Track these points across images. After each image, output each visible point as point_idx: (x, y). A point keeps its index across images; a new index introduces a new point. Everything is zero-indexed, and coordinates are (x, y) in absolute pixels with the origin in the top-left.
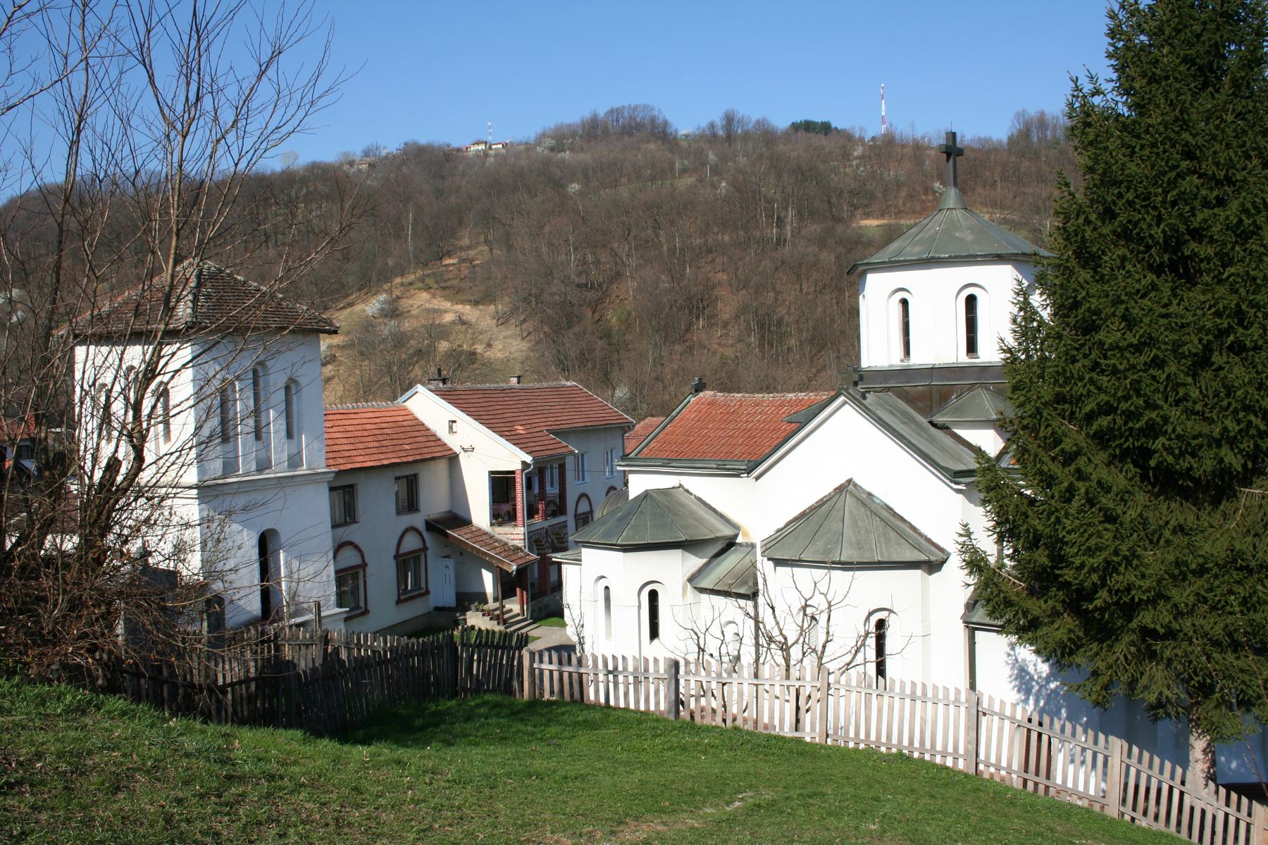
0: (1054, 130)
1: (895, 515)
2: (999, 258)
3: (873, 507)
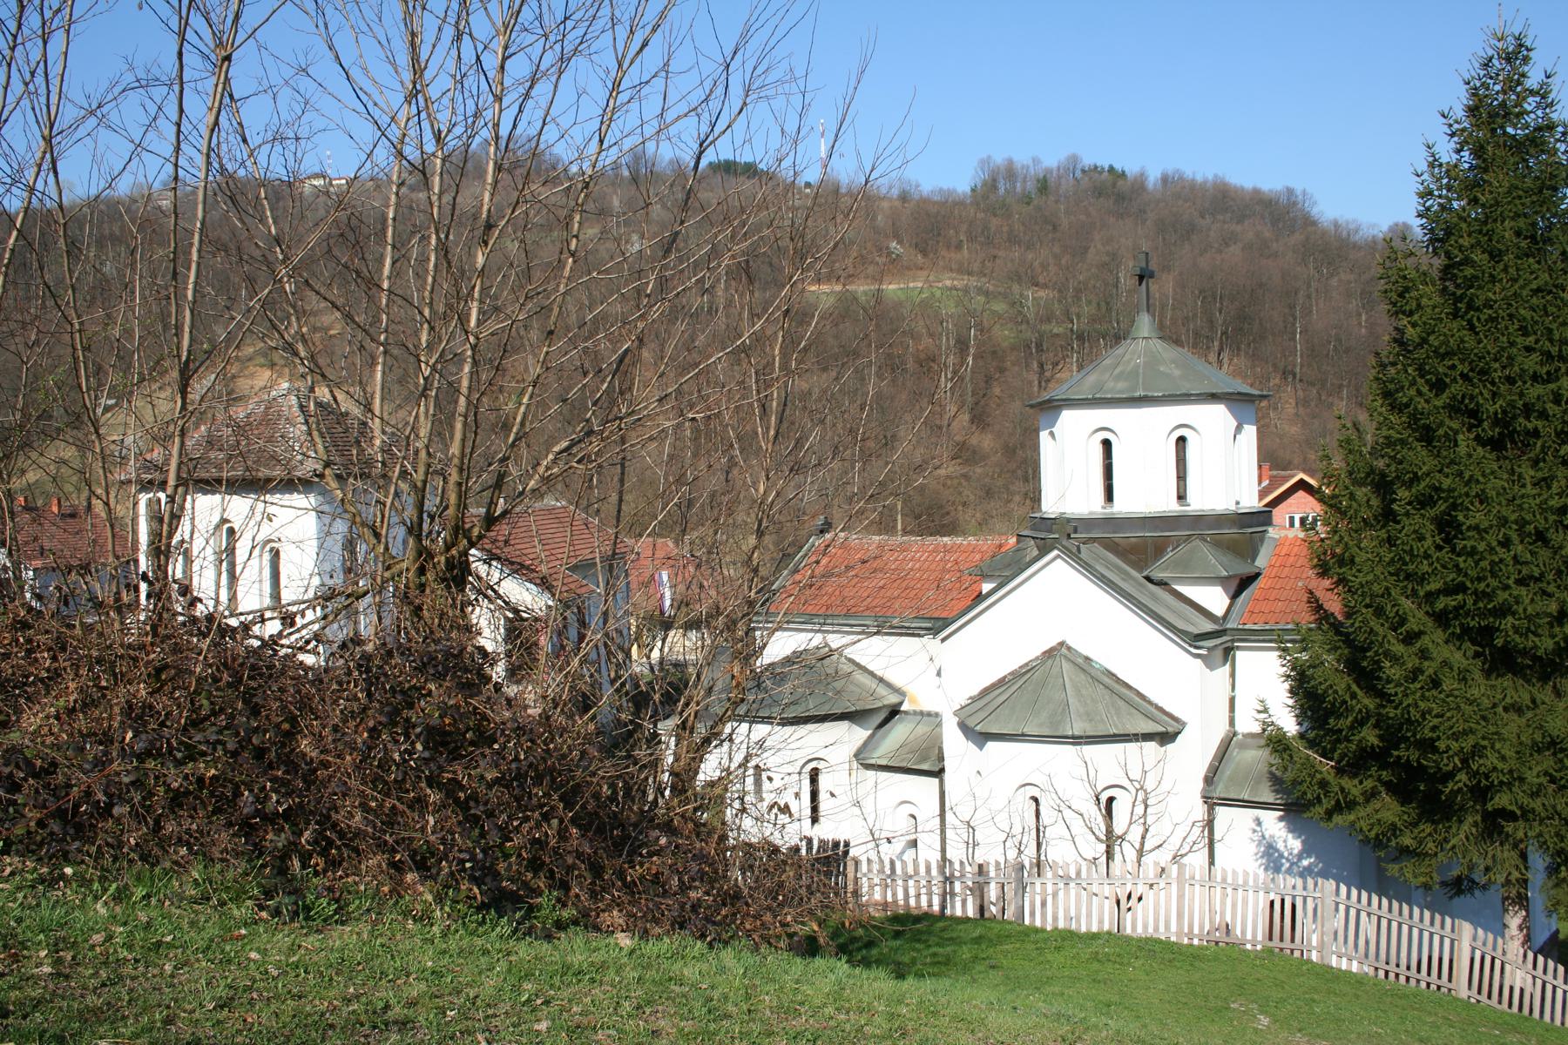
0: (1025, 181)
1: (1118, 680)
2: (1213, 397)
3: (1093, 672)
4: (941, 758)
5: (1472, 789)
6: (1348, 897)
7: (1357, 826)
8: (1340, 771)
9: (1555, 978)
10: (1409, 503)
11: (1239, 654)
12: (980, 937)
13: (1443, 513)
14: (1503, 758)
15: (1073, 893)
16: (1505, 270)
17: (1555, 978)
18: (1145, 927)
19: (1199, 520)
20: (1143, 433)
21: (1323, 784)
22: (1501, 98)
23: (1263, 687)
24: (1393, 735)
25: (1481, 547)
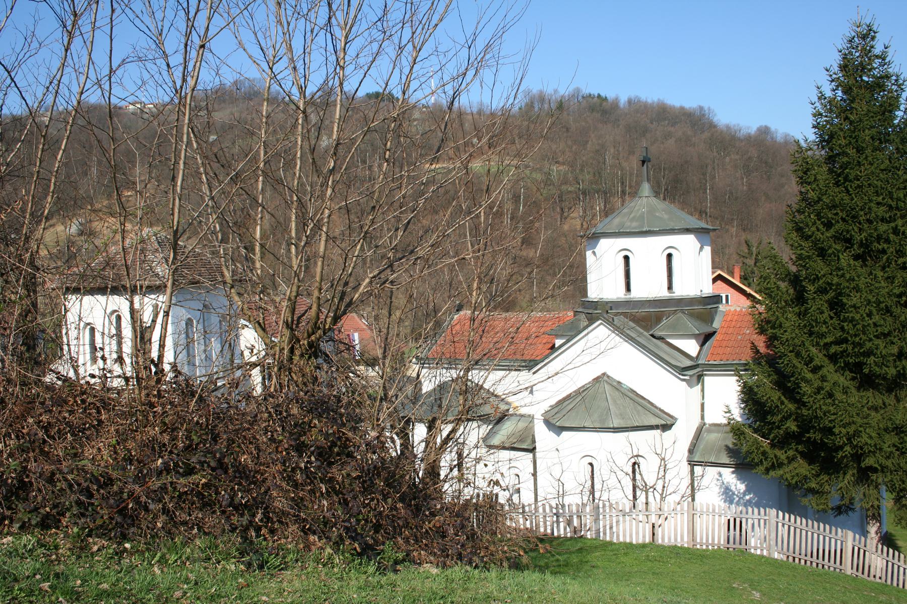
2: (687, 231)
3: (622, 390)
4: (534, 441)
5: (852, 455)
6: (784, 518)
7: (785, 477)
8: (773, 445)
9: (899, 561)
10: (814, 293)
11: (706, 378)
12: (581, 549)
13: (833, 298)
14: (871, 437)
15: (628, 523)
16: (866, 158)
17: (899, 561)
18: (669, 539)
19: (680, 302)
20: (647, 252)
21: (764, 453)
22: (859, 59)
23: (724, 397)
24: (805, 425)
25: (857, 317)
